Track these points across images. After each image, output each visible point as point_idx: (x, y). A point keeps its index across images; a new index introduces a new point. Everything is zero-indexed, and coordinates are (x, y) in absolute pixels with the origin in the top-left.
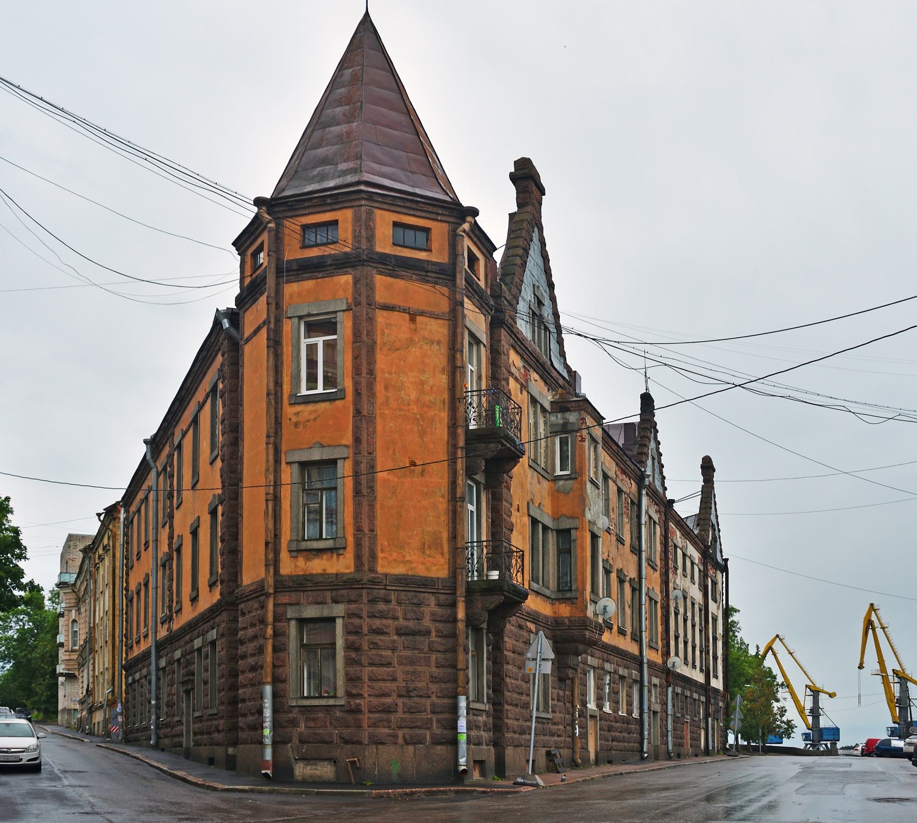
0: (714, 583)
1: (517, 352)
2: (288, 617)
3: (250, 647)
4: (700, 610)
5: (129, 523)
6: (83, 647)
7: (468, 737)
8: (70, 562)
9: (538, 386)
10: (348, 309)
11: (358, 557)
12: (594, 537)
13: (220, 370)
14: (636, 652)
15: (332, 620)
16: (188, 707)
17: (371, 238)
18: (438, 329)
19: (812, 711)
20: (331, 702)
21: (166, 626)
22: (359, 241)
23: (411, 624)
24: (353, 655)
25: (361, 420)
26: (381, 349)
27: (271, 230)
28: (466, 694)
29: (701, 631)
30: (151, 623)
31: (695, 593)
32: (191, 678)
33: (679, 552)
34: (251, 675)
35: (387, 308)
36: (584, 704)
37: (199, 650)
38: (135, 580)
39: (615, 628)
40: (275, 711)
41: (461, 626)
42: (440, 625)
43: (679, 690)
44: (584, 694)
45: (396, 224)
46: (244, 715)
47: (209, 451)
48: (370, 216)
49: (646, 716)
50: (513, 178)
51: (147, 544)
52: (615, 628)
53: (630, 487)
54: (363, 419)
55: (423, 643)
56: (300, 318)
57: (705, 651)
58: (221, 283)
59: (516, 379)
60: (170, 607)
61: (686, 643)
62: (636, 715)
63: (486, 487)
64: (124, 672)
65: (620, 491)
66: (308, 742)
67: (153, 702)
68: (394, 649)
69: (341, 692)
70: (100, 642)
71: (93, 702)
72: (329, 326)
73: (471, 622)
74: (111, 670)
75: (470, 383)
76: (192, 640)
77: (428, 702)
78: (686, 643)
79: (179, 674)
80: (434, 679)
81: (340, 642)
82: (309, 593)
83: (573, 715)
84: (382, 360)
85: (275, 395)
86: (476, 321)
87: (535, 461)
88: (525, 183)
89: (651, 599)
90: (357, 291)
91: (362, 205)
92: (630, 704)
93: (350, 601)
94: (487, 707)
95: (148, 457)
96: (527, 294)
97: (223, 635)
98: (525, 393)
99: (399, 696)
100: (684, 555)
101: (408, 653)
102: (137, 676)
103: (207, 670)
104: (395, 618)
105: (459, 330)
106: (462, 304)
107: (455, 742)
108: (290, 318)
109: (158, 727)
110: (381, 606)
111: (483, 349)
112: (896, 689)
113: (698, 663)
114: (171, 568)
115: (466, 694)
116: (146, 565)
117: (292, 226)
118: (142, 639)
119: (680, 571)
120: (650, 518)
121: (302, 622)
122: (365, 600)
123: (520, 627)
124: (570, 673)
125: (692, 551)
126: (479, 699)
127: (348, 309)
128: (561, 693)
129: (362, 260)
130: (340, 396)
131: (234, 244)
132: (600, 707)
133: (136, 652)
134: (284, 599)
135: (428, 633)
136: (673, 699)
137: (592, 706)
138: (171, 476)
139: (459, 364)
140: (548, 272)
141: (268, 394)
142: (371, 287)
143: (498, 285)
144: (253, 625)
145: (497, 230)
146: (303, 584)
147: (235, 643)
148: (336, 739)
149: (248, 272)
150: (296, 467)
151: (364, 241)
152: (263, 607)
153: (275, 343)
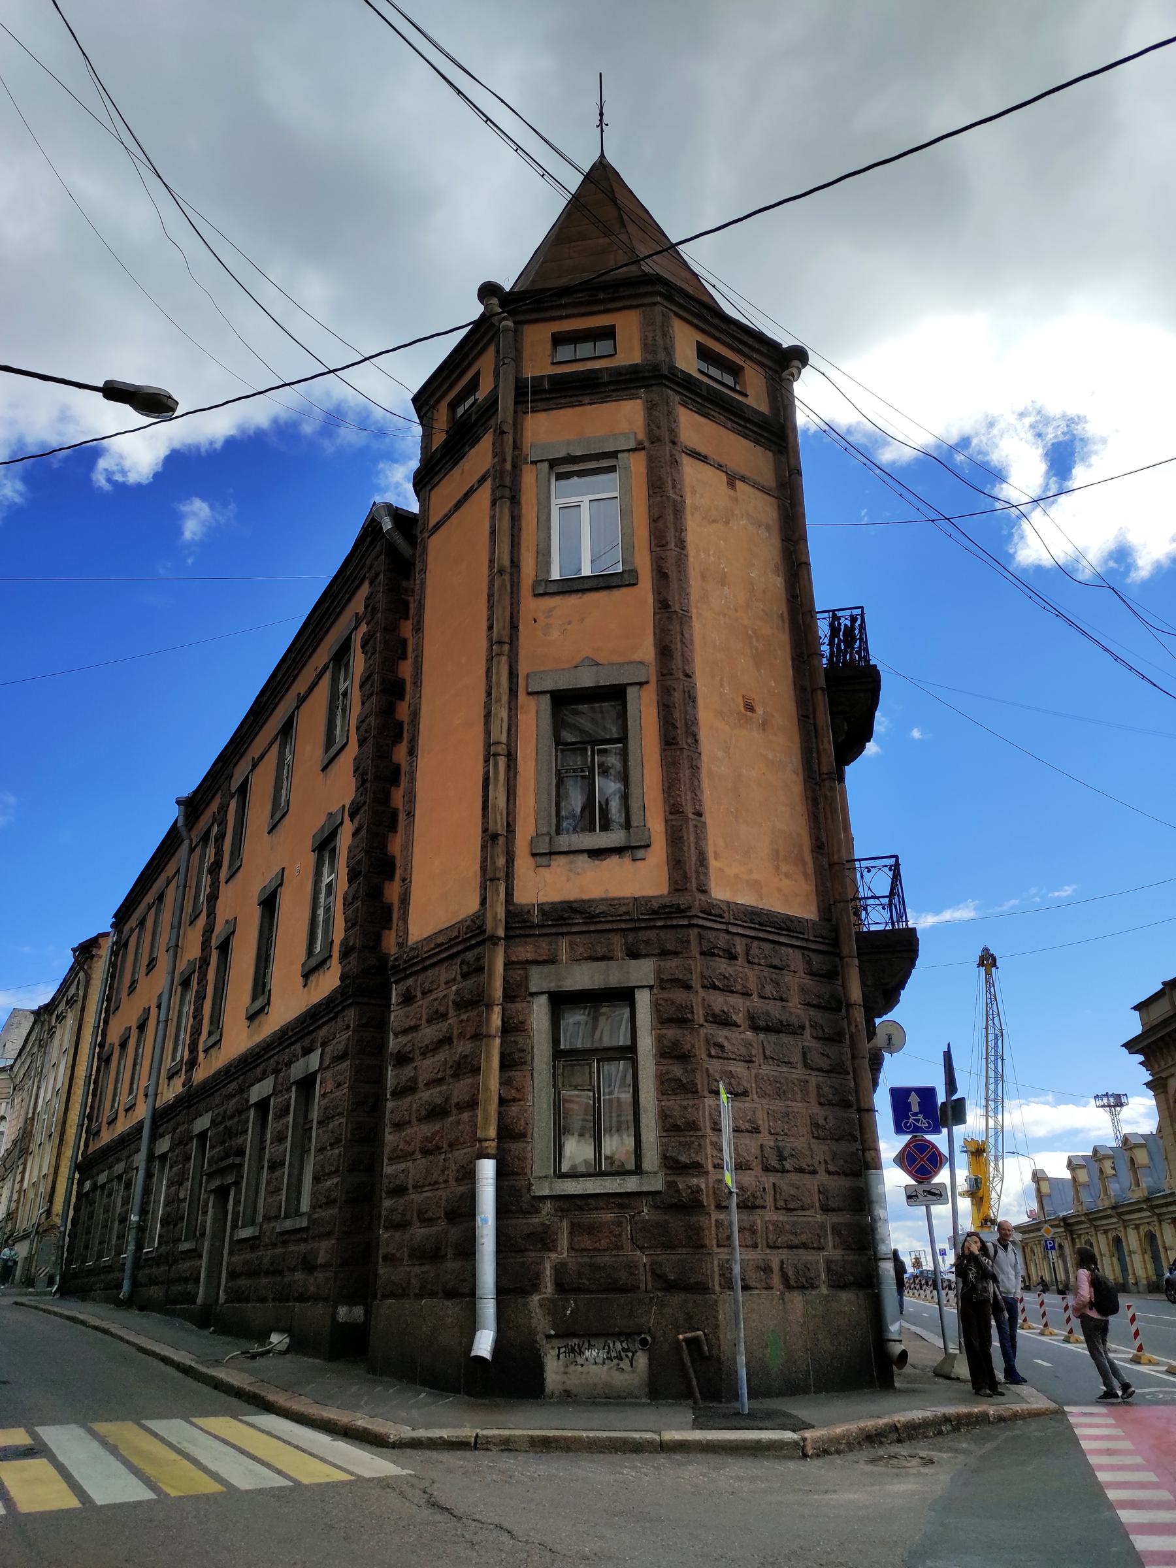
2: (533, 989)
20: (631, 1184)
22: (654, 353)
23: (774, 1009)
24: (677, 1071)
25: (670, 618)
26: (692, 514)
32: (238, 1160)
34: (426, 1129)
35: (696, 455)
40: (502, 1210)
46: (400, 1225)
64: (77, 1176)
66: (579, 1290)
67: (134, 1218)
69: (651, 1160)
70: (39, 1135)
74: (50, 1178)
81: (646, 1044)
82: (578, 939)
91: (656, 304)
93: (664, 954)
95: (180, 824)
99: (767, 1169)
102: (102, 1178)
108: (535, 463)
109: (137, 1264)
110: (722, 966)
117: (537, 336)
118: (121, 1114)
121: (561, 1001)
134: (525, 952)
146: (567, 917)
148: (645, 1279)
150: (546, 700)
152: (478, 969)
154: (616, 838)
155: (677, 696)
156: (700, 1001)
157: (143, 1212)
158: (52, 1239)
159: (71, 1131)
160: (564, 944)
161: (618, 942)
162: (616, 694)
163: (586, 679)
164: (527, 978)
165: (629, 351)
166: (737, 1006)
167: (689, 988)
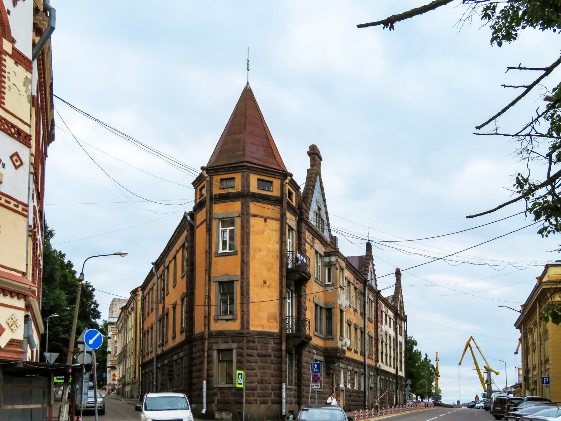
0: (401, 327)
1: (309, 232)
3: (198, 361)
4: (394, 340)
5: (144, 299)
6: (120, 354)
7: (286, 401)
8: (114, 312)
9: (318, 246)
10: (239, 216)
11: (242, 323)
12: (342, 311)
13: (186, 237)
14: (363, 361)
15: (231, 350)
16: (170, 386)
17: (248, 186)
18: (275, 225)
19: (487, 381)
21: (161, 348)
23: (264, 352)
24: (240, 365)
27: (207, 181)
28: (286, 382)
29: (394, 350)
30: (154, 346)
31: (391, 332)
33: (384, 314)
36: (338, 385)
37: (176, 361)
38: (147, 325)
39: (353, 350)
40: (208, 389)
41: (284, 353)
42: (276, 353)
43: (383, 377)
44: (338, 380)
45: (259, 180)
47: (181, 272)
48: (248, 177)
49: (367, 390)
50: (309, 154)
51: (152, 309)
52: (353, 350)
53: (360, 286)
54: (245, 264)
55: (269, 359)
56: (220, 219)
57: (396, 359)
58: (187, 200)
59: (309, 244)
60: (163, 340)
61: (386, 355)
62: (362, 389)
63: (295, 292)
65: (356, 288)
68: (256, 363)
70: (129, 353)
71: (125, 382)
72: (232, 224)
73: (288, 351)
75: (289, 248)
76: (173, 356)
77: (270, 386)
78: (386, 355)
79: (166, 371)
80: (273, 376)
81: (235, 360)
83: (333, 390)
84: (252, 237)
85: (209, 252)
86: (291, 220)
87: (317, 279)
88: (314, 156)
89: (370, 336)
90: (242, 209)
92: (359, 384)
93: (239, 342)
94: (294, 387)
95: (154, 270)
96: (314, 206)
97: (186, 355)
98: (312, 249)
99: (259, 383)
100: (386, 315)
101: (262, 364)
102: (147, 370)
103: (179, 370)
104: (257, 350)
105: (284, 226)
106: (285, 214)
107: (280, 403)
110: (251, 344)
111: (294, 232)
112: (485, 376)
113: (392, 365)
114: (163, 322)
115: (286, 382)
116: (152, 319)
117: (217, 179)
119: (384, 322)
120: (370, 299)
121: (219, 351)
122: (245, 341)
123: (310, 352)
124: (331, 371)
125: (391, 313)
126: (291, 384)
127: (239, 216)
128: (328, 380)
129: (245, 196)
130: (235, 254)
131: (192, 184)
132: (345, 386)
133: (147, 359)
134: (212, 341)
135: (270, 356)
136: (380, 381)
137: (342, 385)
138: (164, 280)
139: (284, 240)
140: (323, 195)
141: (206, 252)
142: (248, 207)
143: (299, 207)
144: (199, 351)
145: (301, 179)
146: (221, 334)
147: (191, 359)
149: (198, 197)
150: (217, 283)
151: (245, 187)
152: (203, 344)
153: (209, 230)
154: (230, 317)
155: (245, 284)
156: (245, 352)
157: (157, 382)
158: (136, 385)
159: (138, 353)
160: (220, 339)
161: (230, 340)
162: (232, 282)
163: (226, 279)
164: (212, 346)
165: (237, 186)
166: (255, 352)
167: (243, 349)
